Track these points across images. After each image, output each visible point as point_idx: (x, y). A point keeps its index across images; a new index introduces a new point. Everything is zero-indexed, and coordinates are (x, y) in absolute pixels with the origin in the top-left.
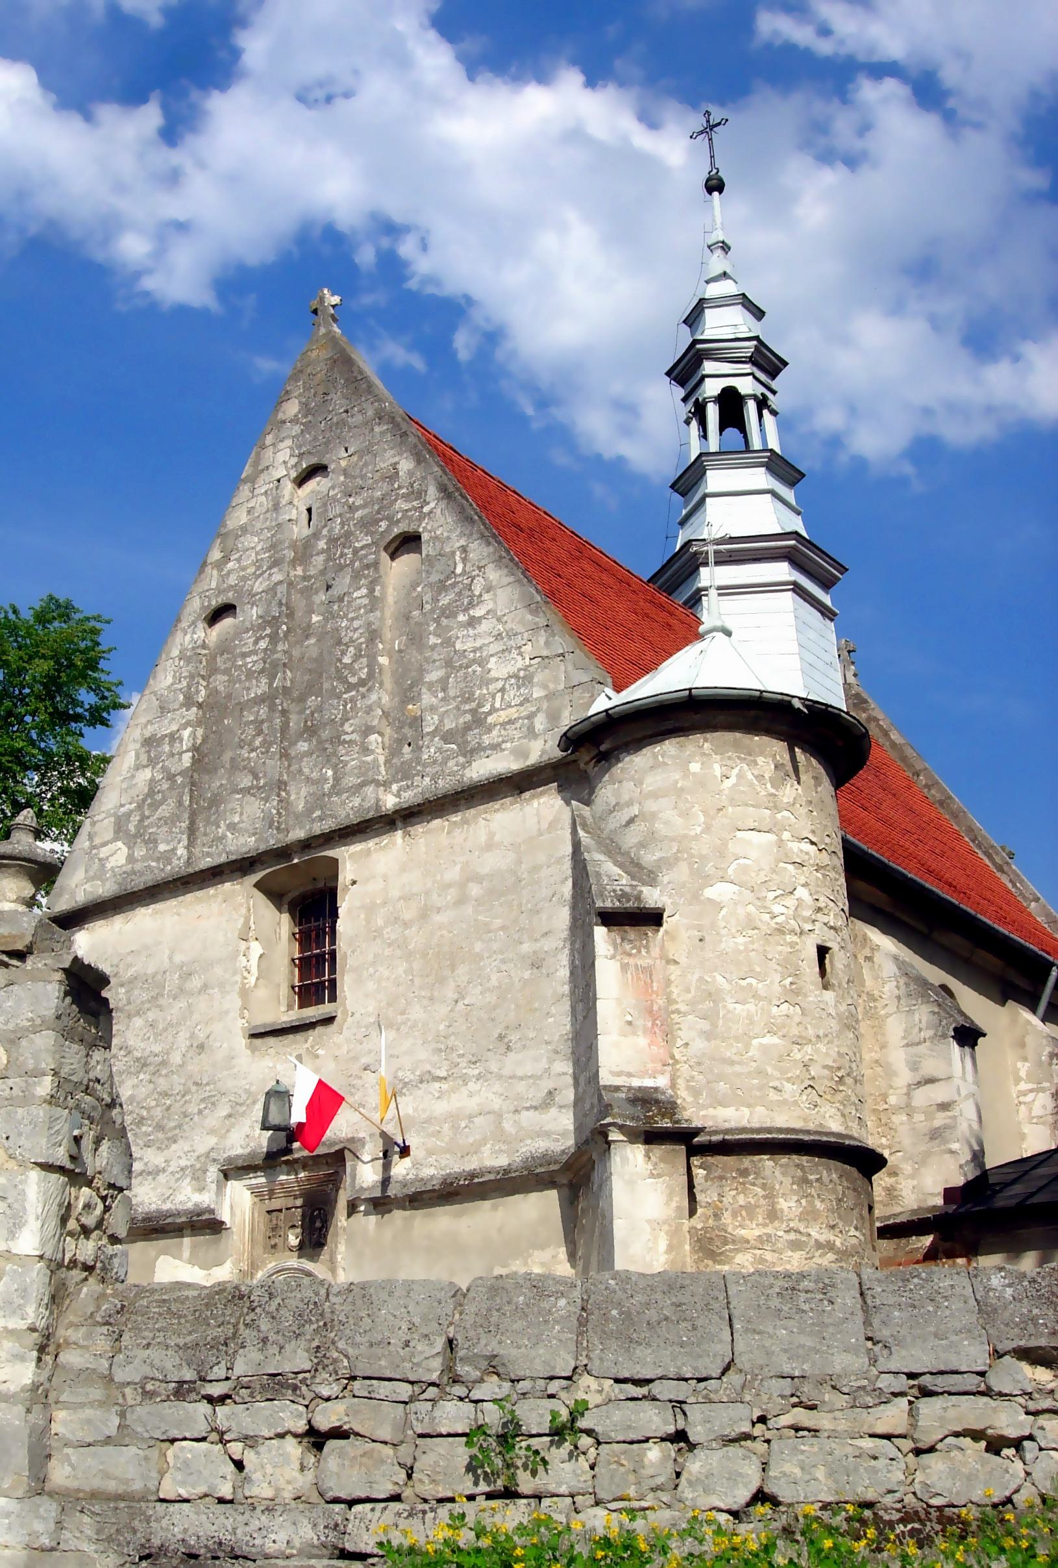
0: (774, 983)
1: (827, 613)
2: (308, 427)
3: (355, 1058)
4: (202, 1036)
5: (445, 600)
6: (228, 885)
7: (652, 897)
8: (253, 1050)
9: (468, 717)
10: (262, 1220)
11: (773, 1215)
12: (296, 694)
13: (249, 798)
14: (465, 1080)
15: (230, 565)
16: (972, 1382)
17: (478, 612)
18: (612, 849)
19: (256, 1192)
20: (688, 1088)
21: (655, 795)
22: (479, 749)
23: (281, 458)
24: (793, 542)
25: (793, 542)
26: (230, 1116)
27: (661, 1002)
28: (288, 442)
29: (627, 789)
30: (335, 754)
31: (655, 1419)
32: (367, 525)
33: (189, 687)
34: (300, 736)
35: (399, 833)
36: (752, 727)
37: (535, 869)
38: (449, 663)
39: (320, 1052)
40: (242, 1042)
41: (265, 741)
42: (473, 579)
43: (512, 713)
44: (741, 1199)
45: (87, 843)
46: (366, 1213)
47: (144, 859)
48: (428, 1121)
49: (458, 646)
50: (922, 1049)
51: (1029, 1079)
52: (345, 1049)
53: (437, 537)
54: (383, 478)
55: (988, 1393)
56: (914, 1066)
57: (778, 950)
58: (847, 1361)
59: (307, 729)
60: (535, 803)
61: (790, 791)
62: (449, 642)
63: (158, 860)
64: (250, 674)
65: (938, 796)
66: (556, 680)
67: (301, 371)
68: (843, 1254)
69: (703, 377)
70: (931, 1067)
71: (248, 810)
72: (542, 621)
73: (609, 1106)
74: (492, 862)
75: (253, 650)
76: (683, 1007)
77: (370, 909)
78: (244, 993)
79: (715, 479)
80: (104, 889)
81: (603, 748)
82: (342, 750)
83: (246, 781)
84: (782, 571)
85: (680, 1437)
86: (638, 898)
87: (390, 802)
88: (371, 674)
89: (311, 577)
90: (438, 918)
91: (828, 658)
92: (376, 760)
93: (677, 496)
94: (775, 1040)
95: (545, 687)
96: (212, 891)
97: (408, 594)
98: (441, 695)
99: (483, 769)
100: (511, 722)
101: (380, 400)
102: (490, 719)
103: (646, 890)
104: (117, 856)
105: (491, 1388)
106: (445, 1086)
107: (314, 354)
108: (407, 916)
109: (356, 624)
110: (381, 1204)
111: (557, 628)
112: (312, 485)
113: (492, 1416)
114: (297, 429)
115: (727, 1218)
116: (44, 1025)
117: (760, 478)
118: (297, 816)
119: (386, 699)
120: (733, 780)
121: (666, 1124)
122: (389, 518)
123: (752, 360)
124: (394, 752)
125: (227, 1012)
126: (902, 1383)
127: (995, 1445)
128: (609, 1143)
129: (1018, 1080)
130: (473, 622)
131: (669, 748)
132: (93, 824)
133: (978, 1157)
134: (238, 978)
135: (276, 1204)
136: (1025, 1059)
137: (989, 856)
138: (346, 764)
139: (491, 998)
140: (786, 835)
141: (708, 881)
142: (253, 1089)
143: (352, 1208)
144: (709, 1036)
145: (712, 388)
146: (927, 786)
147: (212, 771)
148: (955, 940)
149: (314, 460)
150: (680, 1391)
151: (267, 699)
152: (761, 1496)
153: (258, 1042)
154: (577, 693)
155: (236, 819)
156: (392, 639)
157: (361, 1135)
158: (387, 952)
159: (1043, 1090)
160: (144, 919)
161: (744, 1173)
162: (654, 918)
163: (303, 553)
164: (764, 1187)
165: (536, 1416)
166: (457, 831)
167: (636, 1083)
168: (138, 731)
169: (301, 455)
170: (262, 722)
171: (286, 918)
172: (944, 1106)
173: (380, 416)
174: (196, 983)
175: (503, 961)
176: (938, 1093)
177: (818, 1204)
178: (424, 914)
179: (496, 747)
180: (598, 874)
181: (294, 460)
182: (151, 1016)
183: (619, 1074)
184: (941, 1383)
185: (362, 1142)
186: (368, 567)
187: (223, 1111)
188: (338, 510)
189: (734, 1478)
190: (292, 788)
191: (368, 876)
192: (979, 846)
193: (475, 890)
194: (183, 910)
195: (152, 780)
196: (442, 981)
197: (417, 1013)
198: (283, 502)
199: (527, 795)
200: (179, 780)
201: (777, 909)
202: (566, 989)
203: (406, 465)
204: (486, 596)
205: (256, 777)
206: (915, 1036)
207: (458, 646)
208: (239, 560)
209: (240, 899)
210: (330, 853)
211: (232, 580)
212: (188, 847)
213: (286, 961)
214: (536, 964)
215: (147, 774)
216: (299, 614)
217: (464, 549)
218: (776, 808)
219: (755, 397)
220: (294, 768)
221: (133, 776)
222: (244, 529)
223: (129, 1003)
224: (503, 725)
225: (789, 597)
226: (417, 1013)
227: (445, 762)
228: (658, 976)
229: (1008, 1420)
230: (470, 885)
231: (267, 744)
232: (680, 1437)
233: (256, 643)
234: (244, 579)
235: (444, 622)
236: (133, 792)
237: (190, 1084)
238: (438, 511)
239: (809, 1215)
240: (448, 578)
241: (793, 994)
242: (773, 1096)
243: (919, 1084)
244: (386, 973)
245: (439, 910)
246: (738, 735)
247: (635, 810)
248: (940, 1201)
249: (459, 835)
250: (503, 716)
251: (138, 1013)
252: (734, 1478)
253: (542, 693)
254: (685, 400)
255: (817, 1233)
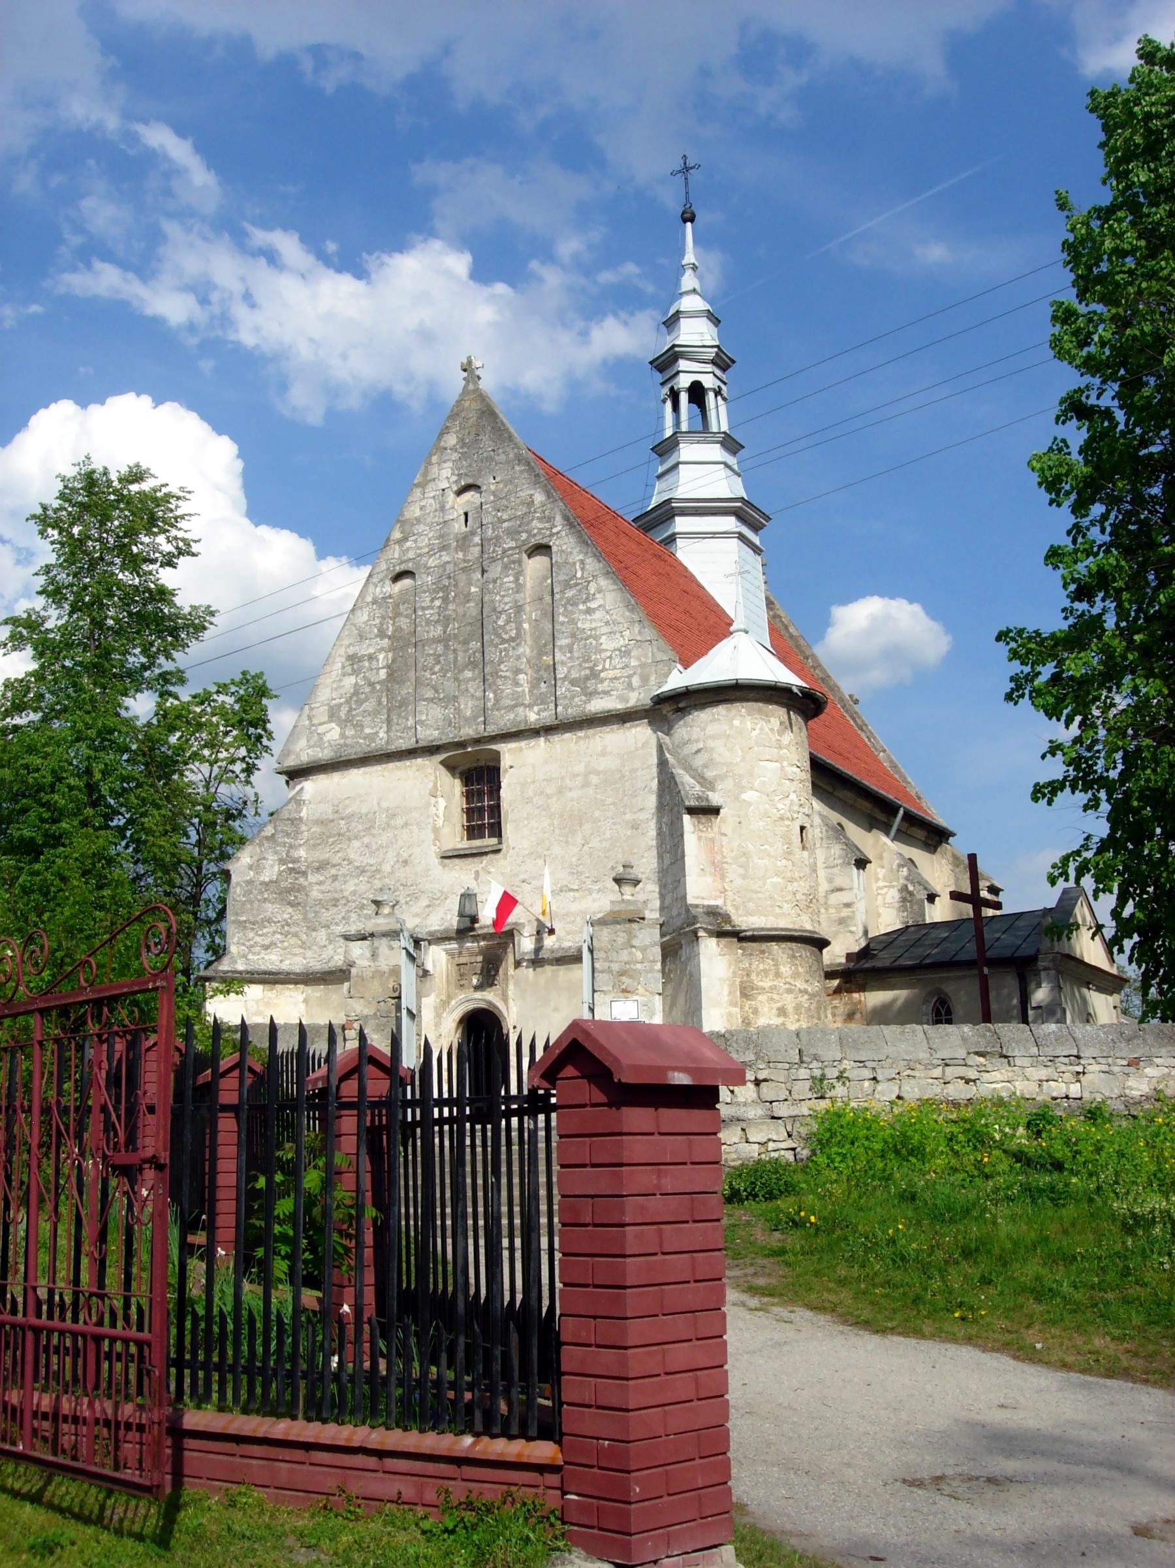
0: (779, 847)
1: (757, 550)
2: (464, 456)
3: (516, 875)
4: (405, 855)
5: (570, 593)
6: (419, 760)
7: (715, 799)
8: (444, 866)
9: (587, 672)
10: (454, 970)
11: (778, 975)
12: (461, 639)
13: (431, 705)
14: (590, 892)
15: (409, 544)
16: (962, 1062)
17: (593, 605)
18: (689, 768)
19: (450, 953)
20: (733, 905)
21: (713, 737)
22: (595, 693)
23: (445, 475)
24: (739, 504)
25: (739, 504)
26: (429, 906)
27: (719, 858)
28: (450, 464)
29: (696, 732)
30: (494, 683)
31: (868, 1074)
32: (513, 533)
33: (381, 624)
34: (466, 667)
35: (542, 739)
36: (768, 700)
37: (633, 771)
38: (573, 635)
39: (492, 870)
40: (437, 861)
41: (442, 669)
42: (589, 582)
43: (617, 673)
44: (761, 967)
45: (307, 722)
46: (527, 967)
47: (353, 737)
48: (567, 914)
49: (580, 625)
50: (835, 870)
51: (884, 880)
52: (509, 869)
53: (562, 551)
54: (523, 503)
55: (965, 1065)
56: (830, 881)
57: (781, 830)
58: (923, 1055)
59: (470, 663)
60: (633, 730)
61: (788, 737)
62: (573, 622)
63: (365, 739)
64: (428, 622)
65: (821, 675)
66: (646, 657)
67: (457, 414)
68: (812, 996)
69: (678, 373)
70: (839, 881)
71: (432, 712)
72: (637, 618)
73: (695, 917)
74: (605, 764)
75: (429, 606)
76: (730, 861)
77: (524, 785)
78: (436, 830)
79: (687, 451)
80: (324, 754)
81: (681, 705)
82: (499, 682)
83: (430, 694)
84: (729, 523)
85: (874, 1079)
86: (707, 800)
87: (533, 717)
88: (518, 635)
89: (469, 561)
90: (570, 795)
91: (757, 583)
92: (523, 691)
93: (655, 456)
94: (779, 880)
95: (639, 660)
96: (408, 763)
97: (541, 583)
98: (568, 655)
99: (597, 705)
100: (616, 678)
101: (518, 448)
102: (602, 675)
103: (710, 794)
104: (333, 733)
105: (815, 1064)
106: (577, 894)
107: (467, 404)
108: (549, 792)
109: (506, 600)
110: (537, 962)
111: (646, 623)
112: (468, 496)
113: (817, 1073)
114: (455, 456)
115: (754, 976)
116: (655, 944)
117: (715, 452)
118: (467, 719)
119: (528, 651)
120: (757, 731)
121: (728, 928)
122: (529, 532)
123: (713, 362)
124: (534, 685)
125: (423, 841)
126: (940, 1062)
127: (968, 1081)
128: (697, 938)
129: (877, 880)
130: (589, 611)
131: (721, 710)
132: (312, 709)
133: (866, 932)
134: (431, 820)
135: (463, 960)
136: (883, 867)
137: (854, 719)
138: (503, 691)
139: (606, 845)
140: (785, 763)
141: (743, 789)
142: (445, 890)
143: (518, 964)
144: (744, 877)
145: (684, 381)
146: (814, 668)
147: (401, 682)
148: (848, 795)
149: (470, 481)
150: (874, 1064)
151: (444, 640)
152: (899, 1097)
153: (447, 861)
154: (660, 666)
155: (424, 718)
156: (531, 613)
157: (522, 921)
158: (537, 812)
159: (893, 887)
160: (356, 777)
161: (763, 952)
162: (715, 811)
163: (464, 542)
164: (773, 960)
165: (832, 1073)
166: (582, 742)
167: (706, 903)
168: (343, 650)
169: (460, 475)
170: (440, 655)
171: (457, 782)
172: (848, 905)
173: (519, 459)
174: (399, 821)
175: (614, 824)
176: (845, 897)
177: (801, 970)
178: (561, 791)
179: (607, 693)
180: (683, 784)
181: (454, 478)
182: (366, 840)
183: (698, 898)
184: (952, 1062)
185: (523, 925)
186: (514, 562)
187: (424, 902)
188: (490, 519)
189: (891, 1091)
190: (462, 700)
191: (520, 765)
192: (847, 711)
193: (594, 779)
194: (386, 774)
195: (356, 684)
196: (573, 832)
197: (557, 850)
198: (448, 506)
199: (628, 725)
200: (378, 687)
201: (780, 806)
202: (654, 843)
203: (539, 497)
204: (598, 596)
205: (437, 692)
206: (831, 862)
207: (580, 625)
208: (415, 541)
209: (429, 770)
210: (494, 747)
211: (411, 555)
212: (387, 732)
213: (459, 810)
214: (635, 826)
215: (352, 680)
216: (461, 585)
217: (582, 562)
218: (780, 747)
219: (714, 390)
220: (463, 687)
221: (340, 680)
222: (418, 520)
223: (348, 831)
224: (612, 680)
225: (735, 543)
226: (557, 850)
227: (573, 697)
228: (717, 844)
229: (972, 1074)
230: (592, 776)
231: (444, 671)
232: (874, 1079)
233: (432, 601)
234: (420, 555)
235: (570, 608)
236: (342, 691)
237: (398, 885)
238: (563, 533)
239: (796, 975)
240: (571, 579)
241: (788, 854)
242: (778, 910)
243: (833, 891)
244: (536, 825)
245: (570, 789)
246: (761, 704)
247: (701, 745)
248: (843, 960)
249: (583, 744)
250: (611, 674)
251: (356, 838)
252: (891, 1091)
253: (637, 663)
254: (662, 384)
255: (800, 984)
